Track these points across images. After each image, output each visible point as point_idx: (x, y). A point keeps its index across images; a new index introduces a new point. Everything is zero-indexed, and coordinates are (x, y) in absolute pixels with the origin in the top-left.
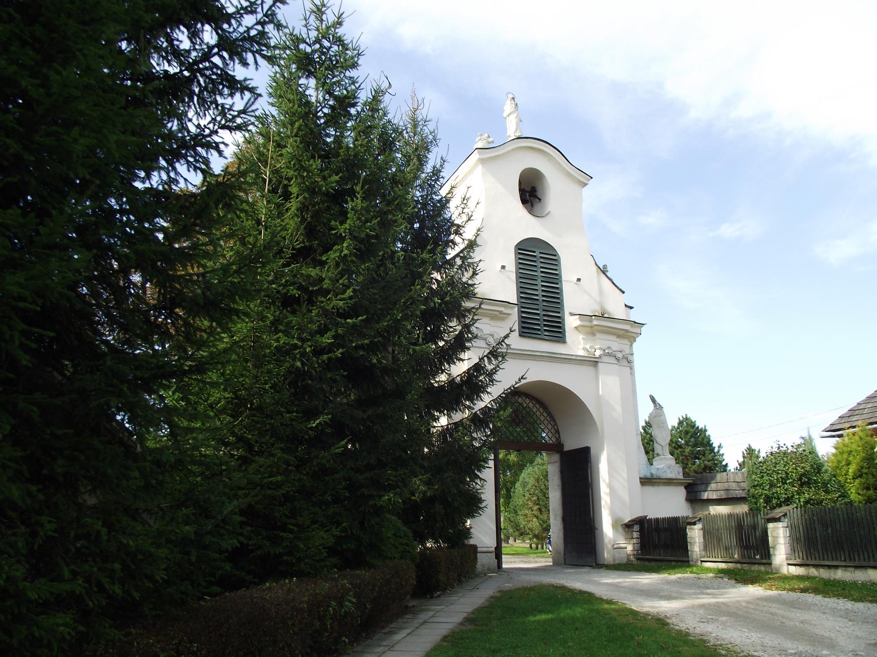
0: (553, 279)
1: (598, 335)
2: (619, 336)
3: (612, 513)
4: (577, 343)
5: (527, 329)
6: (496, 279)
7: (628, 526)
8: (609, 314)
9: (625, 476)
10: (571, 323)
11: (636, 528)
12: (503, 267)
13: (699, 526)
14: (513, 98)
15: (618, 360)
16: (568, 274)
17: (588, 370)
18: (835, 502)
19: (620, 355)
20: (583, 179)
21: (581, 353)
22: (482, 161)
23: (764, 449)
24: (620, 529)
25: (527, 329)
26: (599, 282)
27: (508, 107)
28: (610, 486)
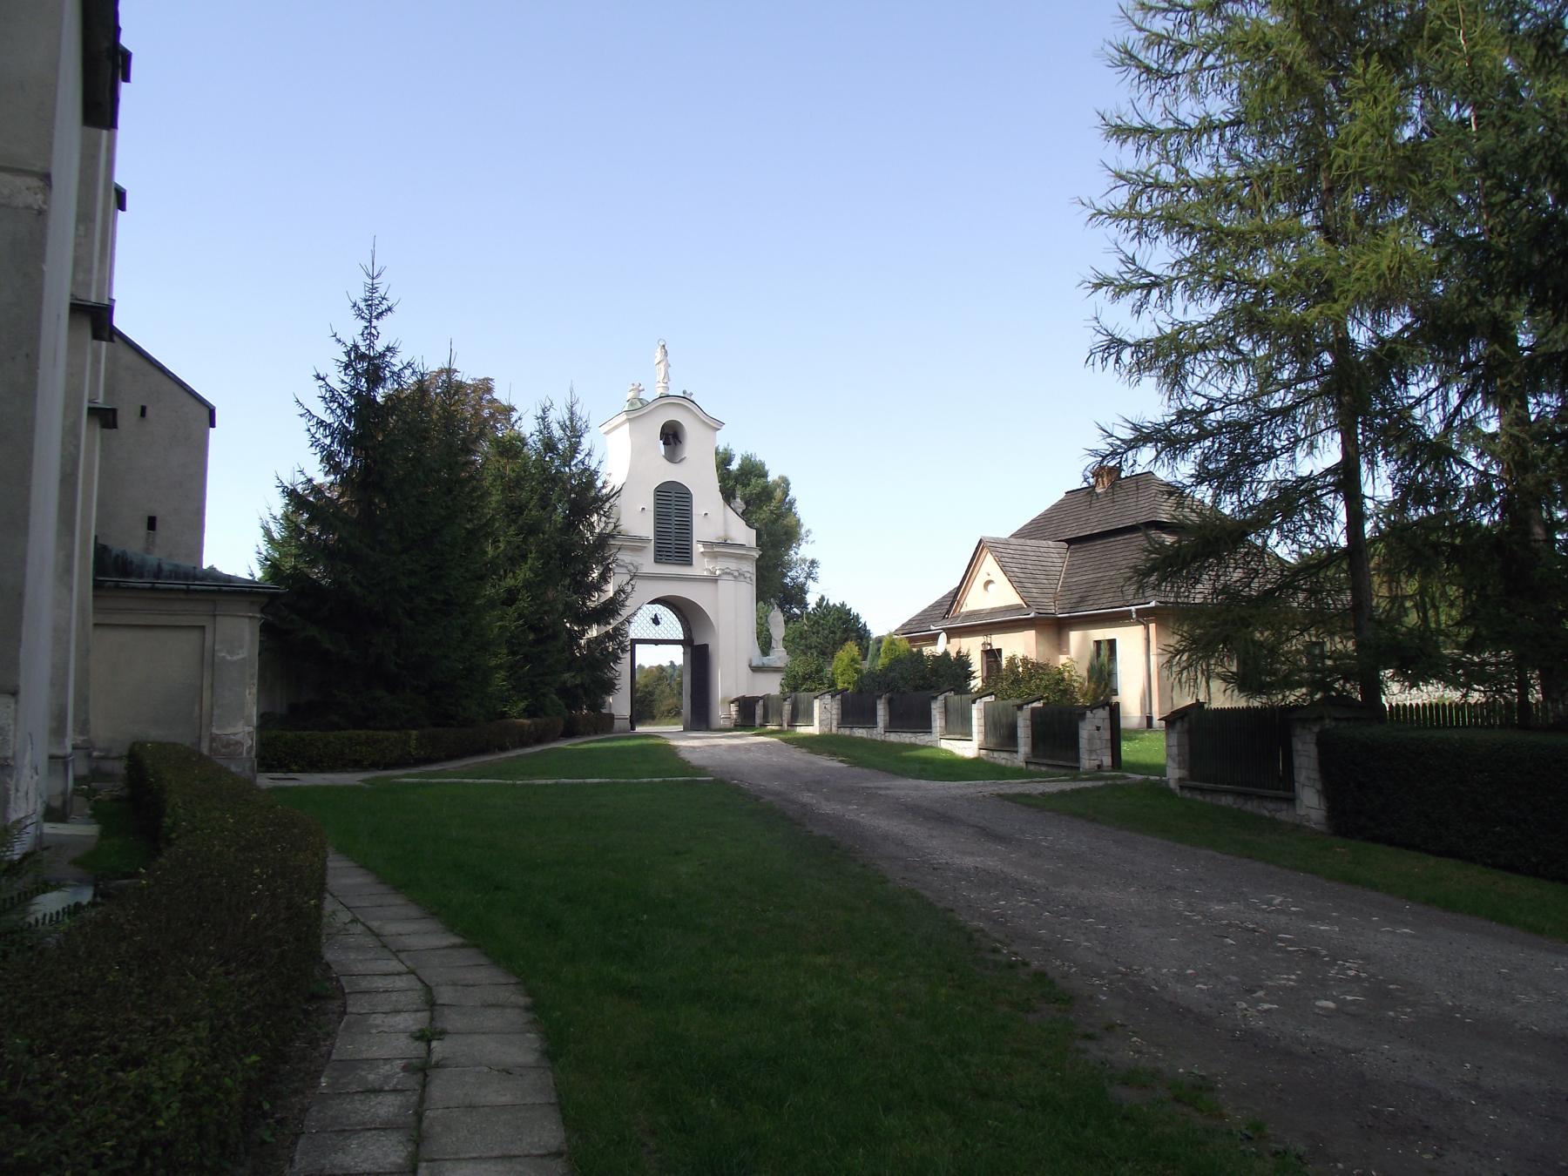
4: (702, 565)
5: (660, 558)
10: (698, 549)
17: (708, 587)
25: (660, 558)
28: (71, 589)
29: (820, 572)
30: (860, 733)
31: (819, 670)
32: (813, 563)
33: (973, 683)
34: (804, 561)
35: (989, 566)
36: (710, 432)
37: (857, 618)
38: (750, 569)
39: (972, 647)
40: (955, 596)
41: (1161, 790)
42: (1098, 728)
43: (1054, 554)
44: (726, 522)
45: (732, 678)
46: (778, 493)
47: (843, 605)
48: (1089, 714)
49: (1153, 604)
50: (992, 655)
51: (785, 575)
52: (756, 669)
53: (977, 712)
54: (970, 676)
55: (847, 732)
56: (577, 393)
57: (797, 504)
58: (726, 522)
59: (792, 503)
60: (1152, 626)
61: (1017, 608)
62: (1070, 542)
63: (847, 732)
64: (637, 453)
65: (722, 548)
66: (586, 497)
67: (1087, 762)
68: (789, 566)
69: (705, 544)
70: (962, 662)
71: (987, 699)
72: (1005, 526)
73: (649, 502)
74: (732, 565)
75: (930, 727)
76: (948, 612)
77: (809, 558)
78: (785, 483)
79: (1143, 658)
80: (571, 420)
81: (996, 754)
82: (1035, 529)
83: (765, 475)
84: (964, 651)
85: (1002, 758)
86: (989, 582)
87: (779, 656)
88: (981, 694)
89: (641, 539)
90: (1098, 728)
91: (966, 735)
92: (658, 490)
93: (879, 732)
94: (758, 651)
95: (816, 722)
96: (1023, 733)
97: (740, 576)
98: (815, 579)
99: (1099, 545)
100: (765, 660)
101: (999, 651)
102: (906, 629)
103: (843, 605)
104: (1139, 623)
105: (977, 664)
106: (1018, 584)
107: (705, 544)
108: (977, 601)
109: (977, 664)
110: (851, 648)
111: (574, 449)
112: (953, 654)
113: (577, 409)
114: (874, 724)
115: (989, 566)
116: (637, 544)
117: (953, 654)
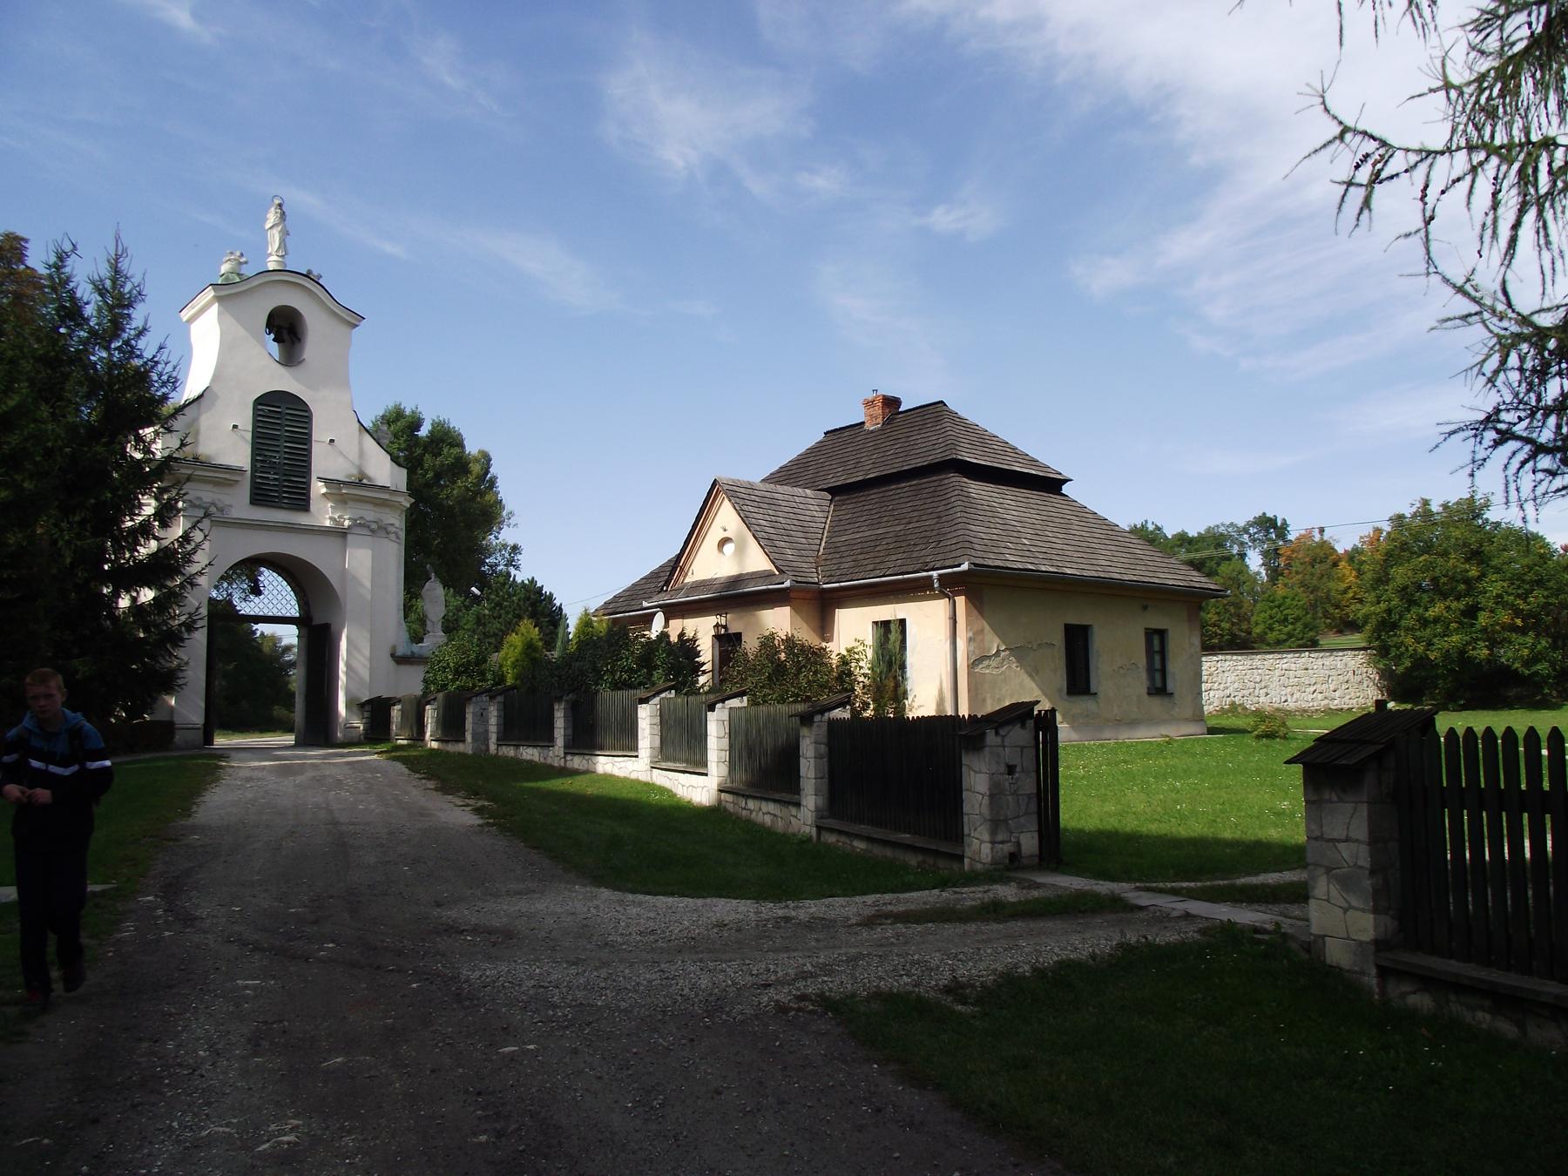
0: (303, 440)
1: (351, 504)
2: (376, 505)
3: (347, 694)
4: (324, 513)
5: (260, 496)
6: (227, 441)
7: (362, 706)
8: (369, 479)
9: (367, 653)
10: (318, 488)
11: (368, 708)
12: (235, 427)
13: (398, 707)
14: (280, 205)
15: (373, 531)
16: (321, 433)
17: (333, 543)
18: (1493, 643)
19: (374, 526)
20: (352, 320)
21: (328, 523)
22: (218, 299)
23: (1453, 499)
24: (355, 709)
25: (260, 496)
26: (360, 443)
27: (272, 217)
28: (348, 665)
29: (522, 559)
30: (530, 754)
31: (481, 660)
32: (515, 549)
33: (702, 680)
34: (505, 546)
35: (726, 518)
36: (343, 329)
37: (550, 598)
38: (397, 521)
39: (703, 630)
40: (676, 565)
41: (1297, 968)
42: (1011, 770)
43: (813, 505)
44: (361, 454)
45: (357, 664)
46: (476, 468)
47: (533, 581)
48: (991, 737)
49: (965, 567)
50: (727, 642)
51: (484, 563)
52: (401, 660)
53: (716, 726)
54: (696, 669)
55: (509, 752)
56: (126, 240)
57: (499, 483)
58: (361, 454)
59: (492, 482)
60: (961, 601)
61: (766, 576)
62: (834, 491)
63: (509, 752)
64: (227, 348)
65: (352, 489)
66: (136, 396)
67: (980, 846)
68: (487, 551)
69: (328, 482)
70: (687, 648)
71: (735, 703)
72: (754, 470)
73: (245, 420)
74: (370, 514)
75: (636, 749)
76: (667, 583)
77: (511, 543)
78: (486, 459)
79: (947, 646)
80: (114, 281)
81: (751, 804)
82: (788, 475)
83: (461, 445)
84: (689, 634)
85: (764, 812)
86: (724, 542)
87: (435, 638)
88: (719, 694)
89: (228, 469)
90: (1011, 770)
91: (697, 765)
92: (261, 401)
93: (935, 574)
94: (405, 636)
95: (469, 738)
96: (809, 768)
97: (377, 530)
98: (517, 568)
99: (874, 494)
100: (416, 648)
101: (738, 636)
102: (609, 607)
103: (533, 581)
104: (943, 595)
105: (706, 652)
106: (768, 545)
107: (328, 482)
108: (712, 565)
109: (706, 652)
110: (528, 630)
111: (117, 326)
112: (674, 638)
113: (124, 265)
114: (549, 740)
115: (726, 518)
116: (223, 475)
117: (674, 638)
